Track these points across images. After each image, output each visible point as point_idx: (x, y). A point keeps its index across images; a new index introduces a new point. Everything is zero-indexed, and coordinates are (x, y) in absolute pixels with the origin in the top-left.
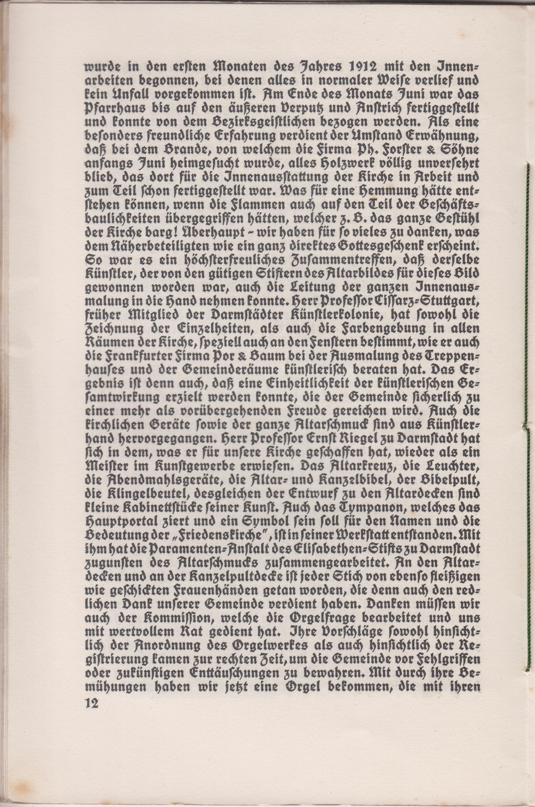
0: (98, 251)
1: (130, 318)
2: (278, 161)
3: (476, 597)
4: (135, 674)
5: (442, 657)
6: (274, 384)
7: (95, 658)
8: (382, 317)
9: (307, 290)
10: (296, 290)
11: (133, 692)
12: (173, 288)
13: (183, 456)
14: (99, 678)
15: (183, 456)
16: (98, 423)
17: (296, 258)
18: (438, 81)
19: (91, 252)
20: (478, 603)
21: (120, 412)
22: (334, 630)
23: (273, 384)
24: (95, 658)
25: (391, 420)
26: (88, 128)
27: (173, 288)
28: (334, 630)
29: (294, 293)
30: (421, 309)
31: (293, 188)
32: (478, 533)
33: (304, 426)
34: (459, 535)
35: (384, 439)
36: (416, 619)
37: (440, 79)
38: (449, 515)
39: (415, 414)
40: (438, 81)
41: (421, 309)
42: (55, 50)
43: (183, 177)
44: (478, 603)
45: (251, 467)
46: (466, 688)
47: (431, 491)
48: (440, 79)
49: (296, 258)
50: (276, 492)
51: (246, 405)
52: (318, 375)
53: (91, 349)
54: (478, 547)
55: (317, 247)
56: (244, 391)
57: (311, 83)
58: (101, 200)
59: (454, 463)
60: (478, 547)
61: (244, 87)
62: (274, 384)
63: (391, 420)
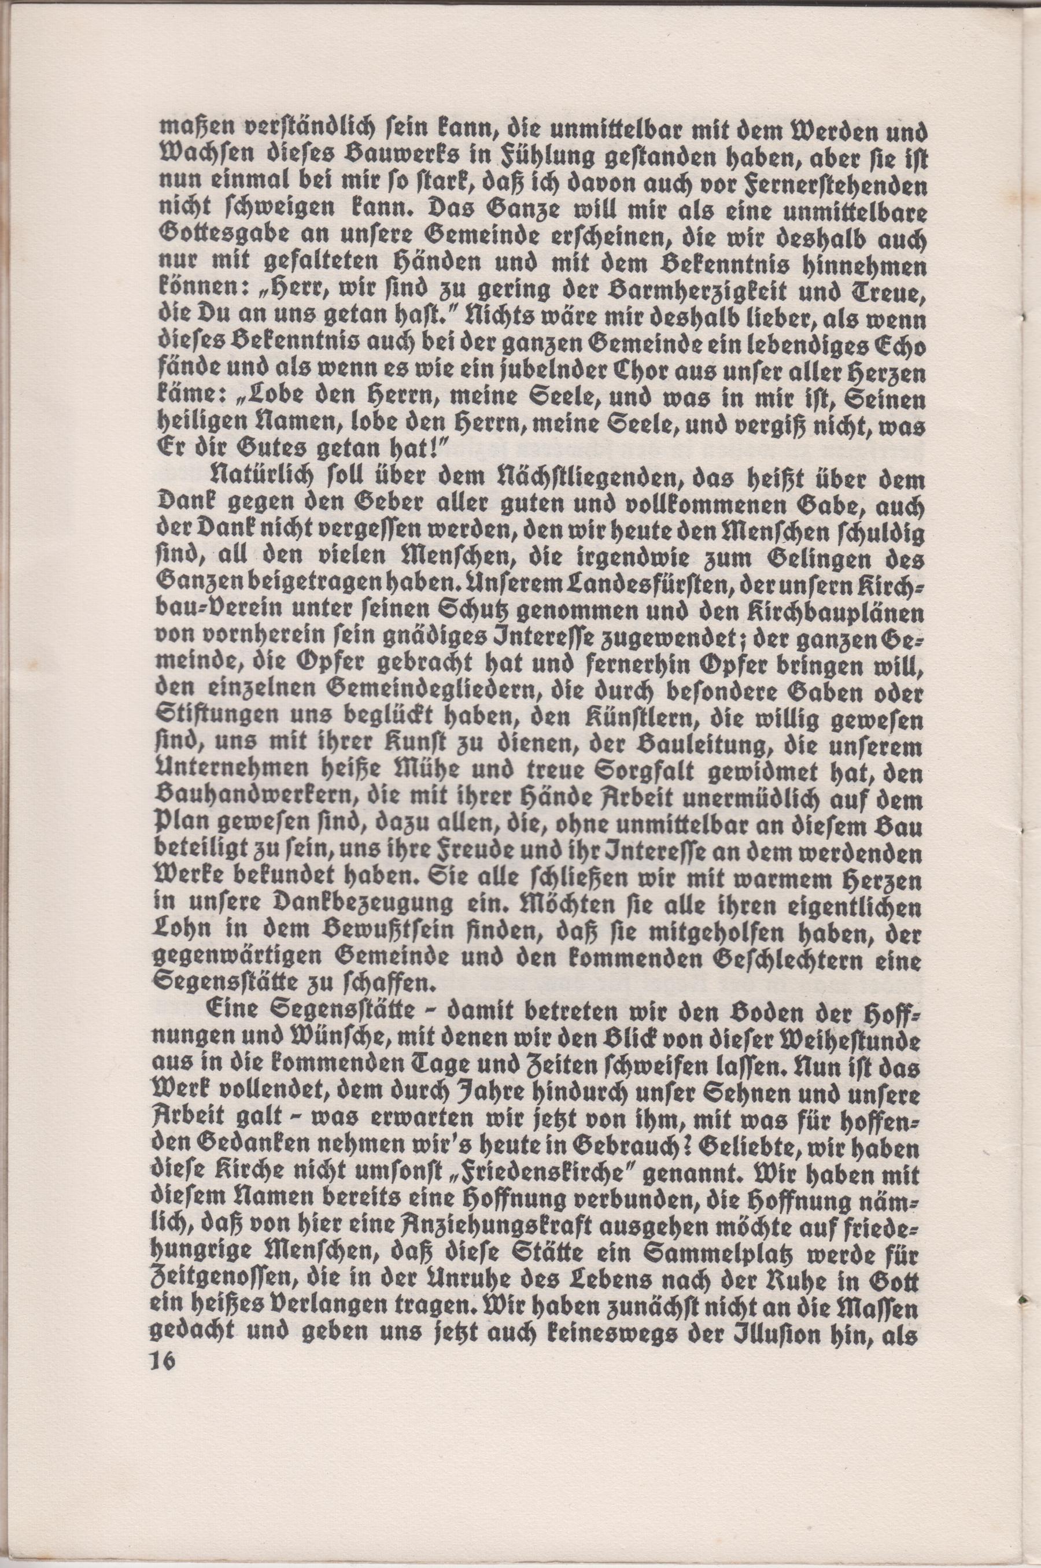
0: (558, 779)
1: (524, 910)
2: (380, 1033)
6: (221, 1010)
7: (788, 423)
8: (923, 299)
11: (317, 1340)
19: (168, 697)
20: (914, 1254)
21: (686, 880)
23: (219, 1010)
24: (788, 423)
25: (721, 416)
26: (836, 758)
30: (701, 682)
32: (916, 1172)
34: (467, 583)
35: (614, 1309)
36: (808, 775)
38: (825, 1083)
41: (701, 682)
42: (104, 94)
43: (805, 1121)
44: (914, 1254)
45: (652, 293)
46: (488, 799)
51: (857, 842)
52: (576, 888)
53: (170, 298)
55: (570, 1174)
61: (814, 385)
62: (221, 1010)
63: (721, 416)
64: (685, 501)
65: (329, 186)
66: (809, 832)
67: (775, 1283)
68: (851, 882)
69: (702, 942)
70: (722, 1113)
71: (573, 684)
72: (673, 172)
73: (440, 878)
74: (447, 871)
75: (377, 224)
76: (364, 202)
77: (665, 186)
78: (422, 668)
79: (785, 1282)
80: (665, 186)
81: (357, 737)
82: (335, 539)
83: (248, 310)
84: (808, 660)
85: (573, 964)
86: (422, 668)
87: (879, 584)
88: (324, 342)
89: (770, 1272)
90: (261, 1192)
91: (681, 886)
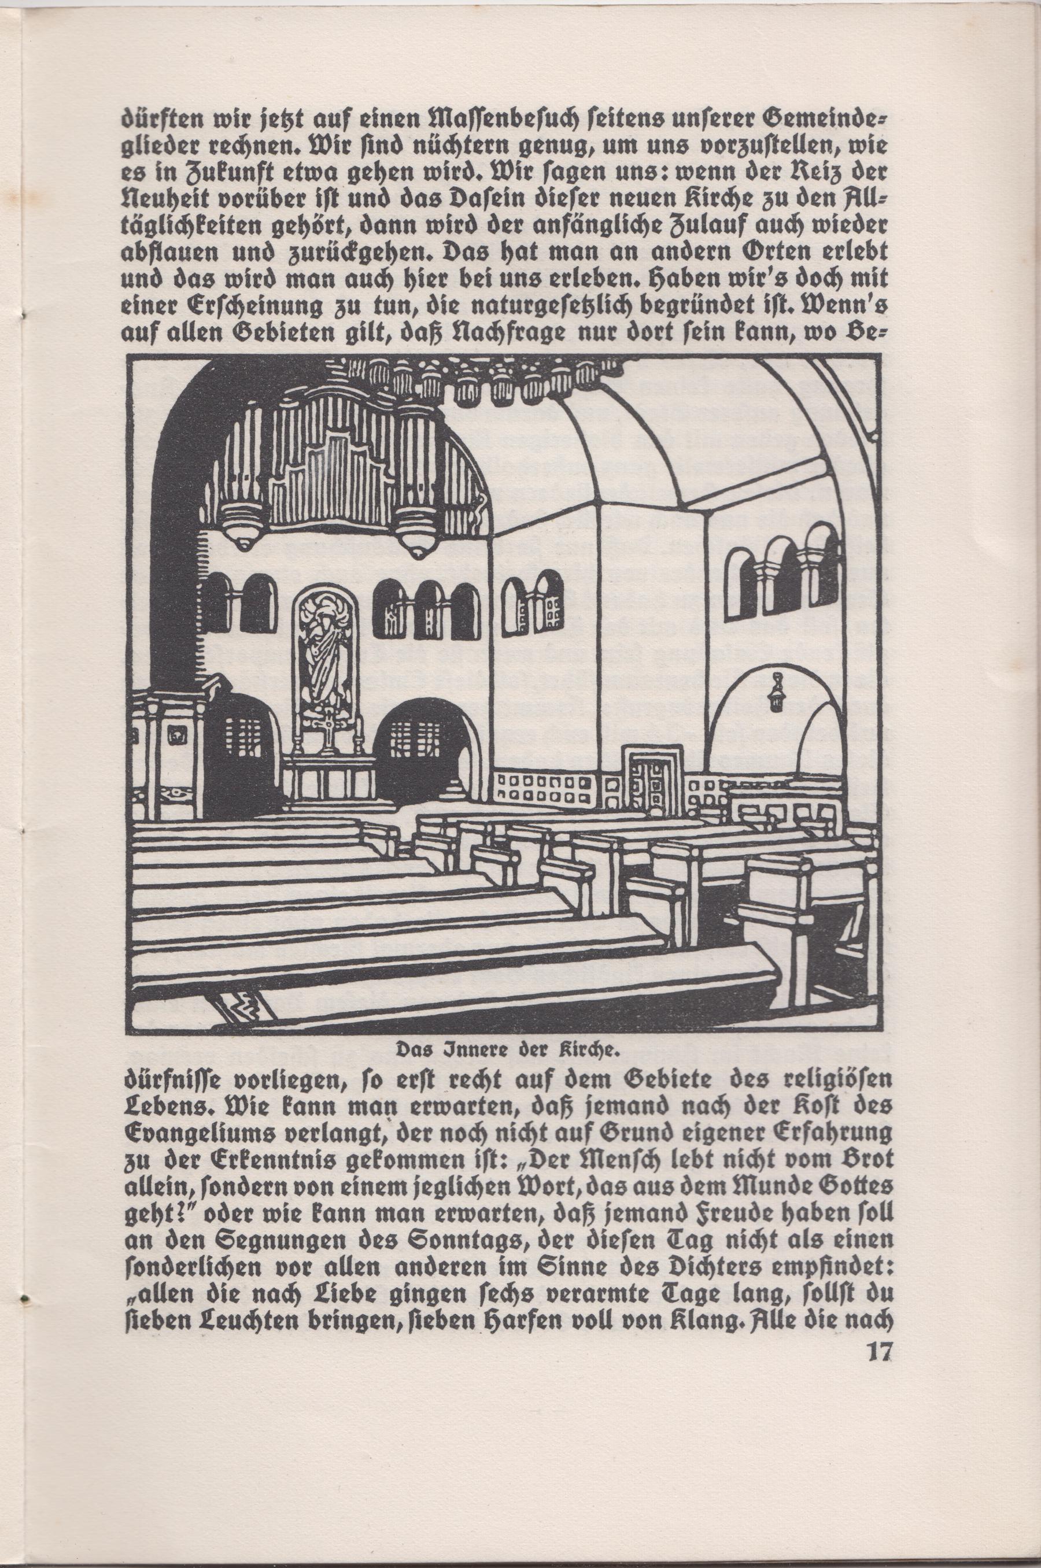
3: (879, 132)
4: (226, 174)
5: (709, 220)
9: (612, 124)
10: (136, 1113)
12: (460, 174)
13: (828, 1248)
14: (694, 288)
15: (828, 1248)
16: (715, 195)
17: (195, 170)
18: (279, 1082)
22: (549, 1183)
27: (460, 174)
28: (549, 1183)
29: (132, 1119)
31: (543, 1181)
32: (884, 274)
33: (862, 200)
37: (283, 1078)
39: (468, 179)
40: (279, 1082)
47: (232, 141)
48: (283, 1078)
49: (195, 170)
50: (183, 142)
54: (884, 247)
56: (295, 187)
57: (808, 257)
58: (377, 163)
59: (242, 141)
60: (884, 247)
64: (390, 1156)
65: (489, 284)
66: (224, 1300)
67: (799, 173)
68: (657, 280)
69: (534, 155)
70: (879, 272)
71: (448, 299)
72: (468, 1122)
73: (550, 1268)
74: (557, 1262)
75: (629, 1231)
76: (746, 327)
77: (460, 1135)
78: (560, 1193)
79: (809, 172)
80: (460, 1135)
81: (739, 115)
82: (698, 290)
83: (404, 1264)
84: (359, 1181)
85: (739, 338)
86: (560, 1193)
87: (705, 195)
88: (300, 1162)
89: (795, 163)
90: (717, 221)
91: (367, 313)
